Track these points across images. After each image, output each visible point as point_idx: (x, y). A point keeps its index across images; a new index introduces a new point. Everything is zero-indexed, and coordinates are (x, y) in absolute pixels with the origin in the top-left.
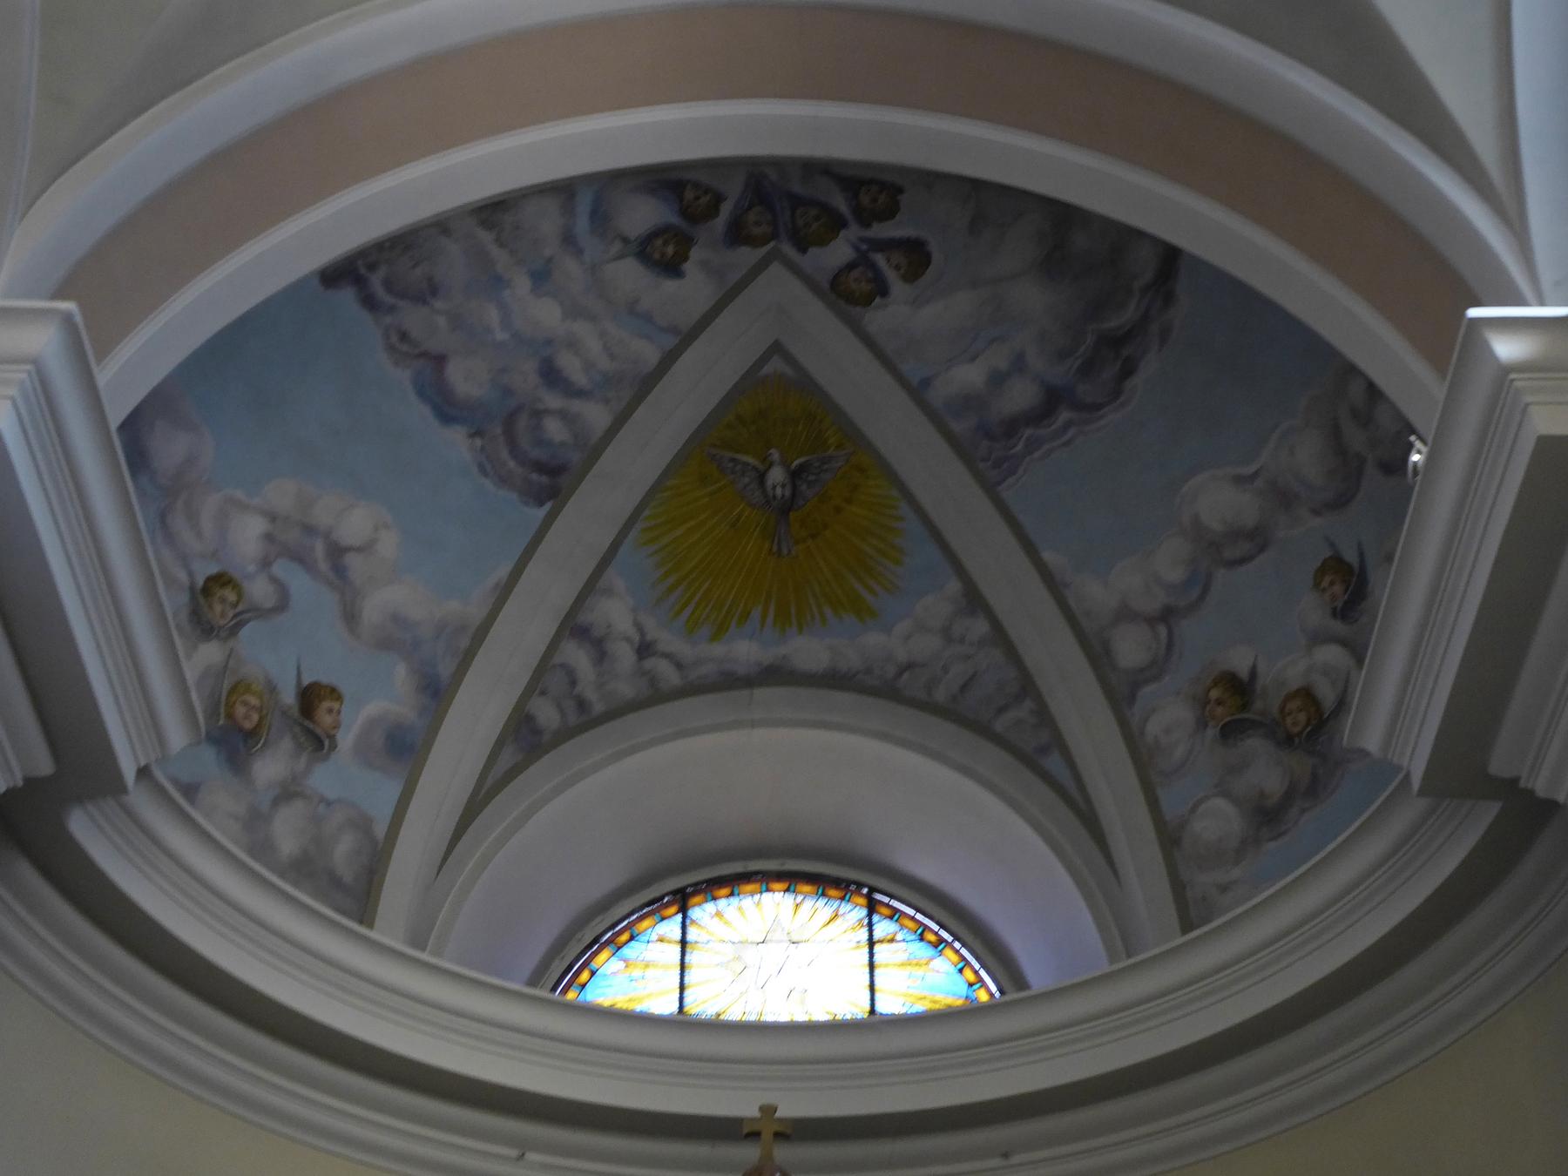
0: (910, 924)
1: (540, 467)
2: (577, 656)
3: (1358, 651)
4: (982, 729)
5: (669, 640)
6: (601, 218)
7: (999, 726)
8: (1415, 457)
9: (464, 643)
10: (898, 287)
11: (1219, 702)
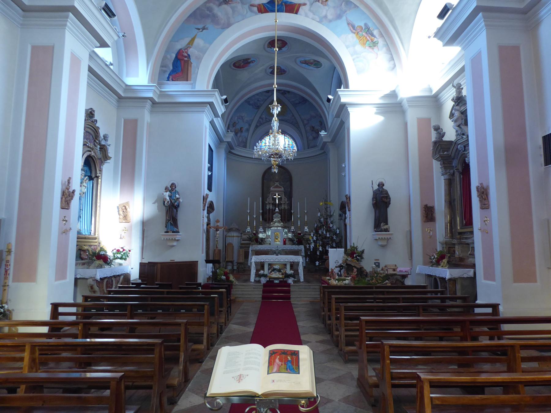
2: (261, 120)
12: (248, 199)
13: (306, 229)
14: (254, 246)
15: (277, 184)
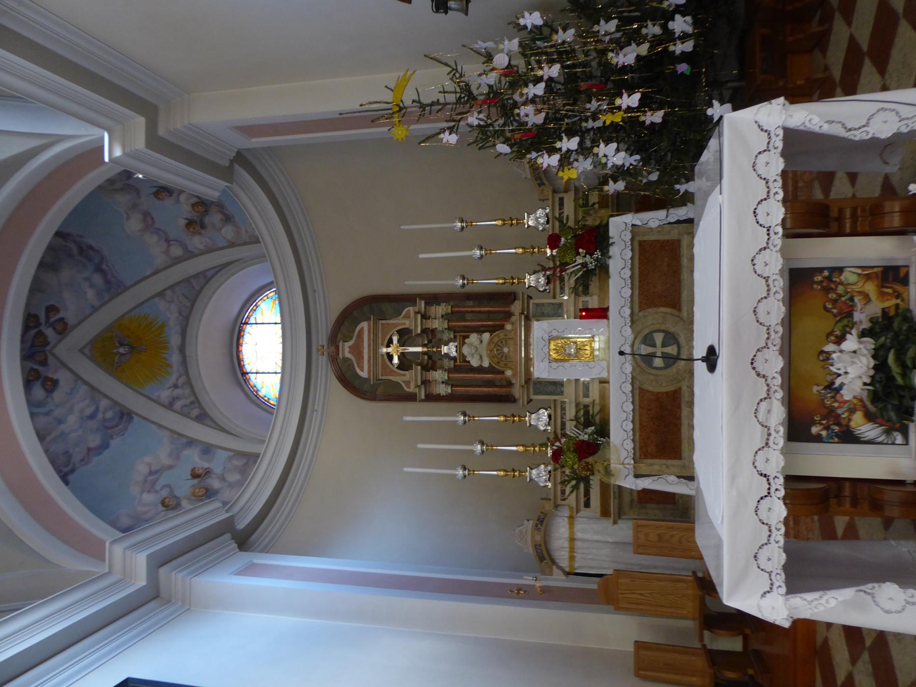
0: (251, 313)
1: (121, 418)
2: (178, 405)
3: (181, 192)
4: (199, 293)
5: (172, 380)
6: (40, 404)
7: (197, 288)
8: (141, 176)
9: (176, 436)
10: (61, 315)
11: (194, 229)
12: (408, 473)
13: (537, 219)
14: (613, 466)
15: (347, 350)
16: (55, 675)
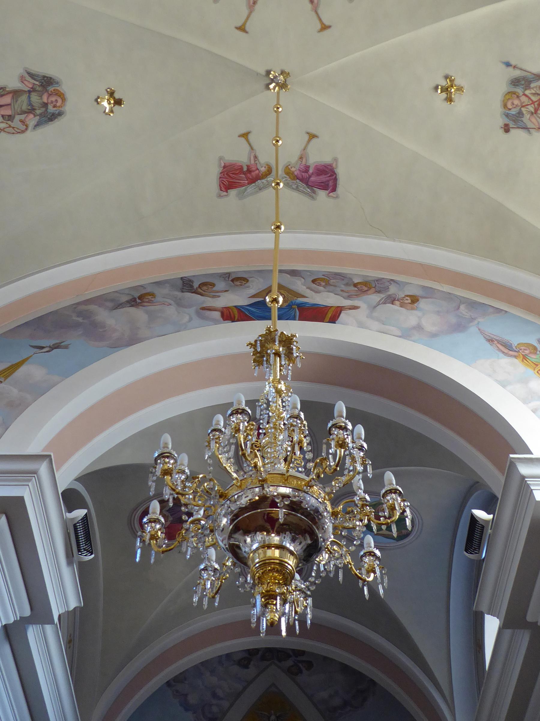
10: (304, 671)
16: (7, 691)
